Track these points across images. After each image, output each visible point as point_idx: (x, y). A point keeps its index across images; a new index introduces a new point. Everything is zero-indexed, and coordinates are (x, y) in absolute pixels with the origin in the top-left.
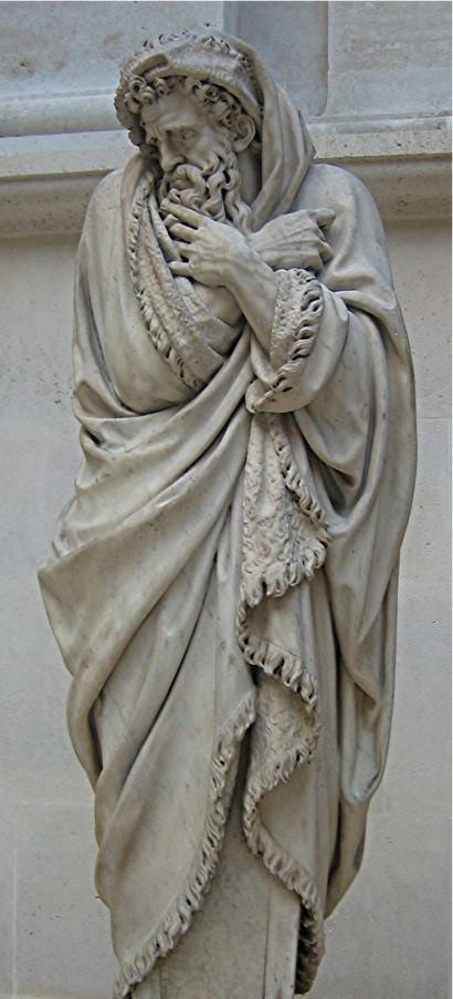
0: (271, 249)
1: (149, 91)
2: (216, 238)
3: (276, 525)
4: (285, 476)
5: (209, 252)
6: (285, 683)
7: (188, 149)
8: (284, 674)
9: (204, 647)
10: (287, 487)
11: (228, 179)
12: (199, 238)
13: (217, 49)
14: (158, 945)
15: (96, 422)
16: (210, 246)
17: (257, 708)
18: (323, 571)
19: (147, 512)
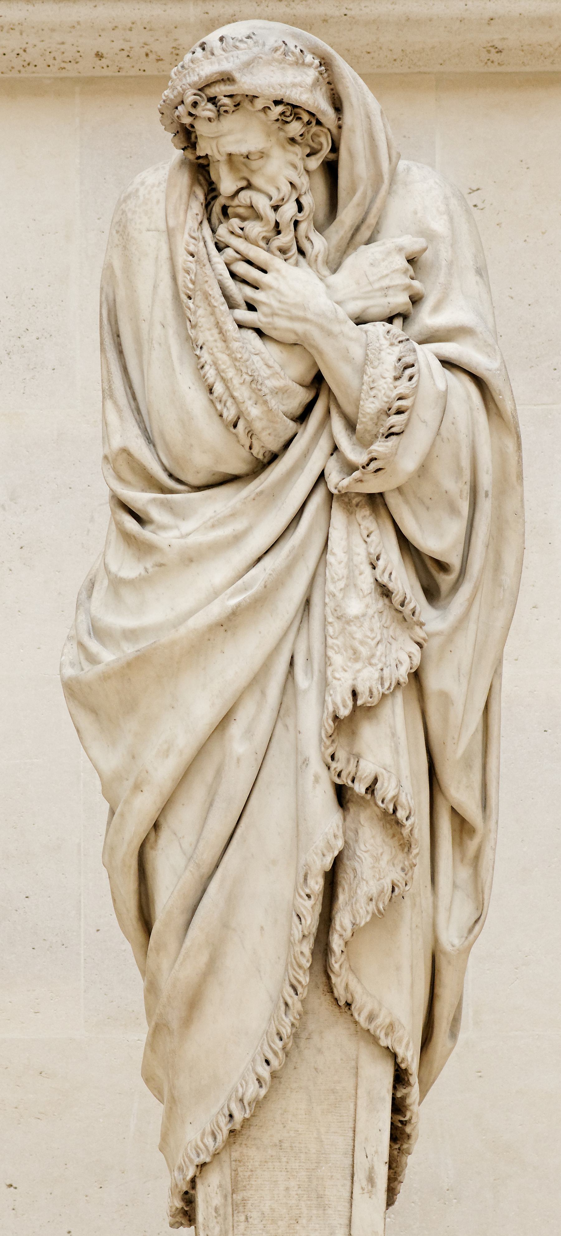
0: (355, 299)
1: (210, 110)
2: (294, 287)
3: (366, 624)
4: (374, 568)
5: (285, 307)
6: (380, 803)
7: (253, 171)
8: (379, 794)
9: (279, 765)
10: (376, 580)
11: (300, 208)
12: (271, 288)
13: (291, 58)
14: (231, 1116)
15: (140, 498)
16: (283, 299)
17: (344, 833)
18: (416, 676)
19: (216, 610)
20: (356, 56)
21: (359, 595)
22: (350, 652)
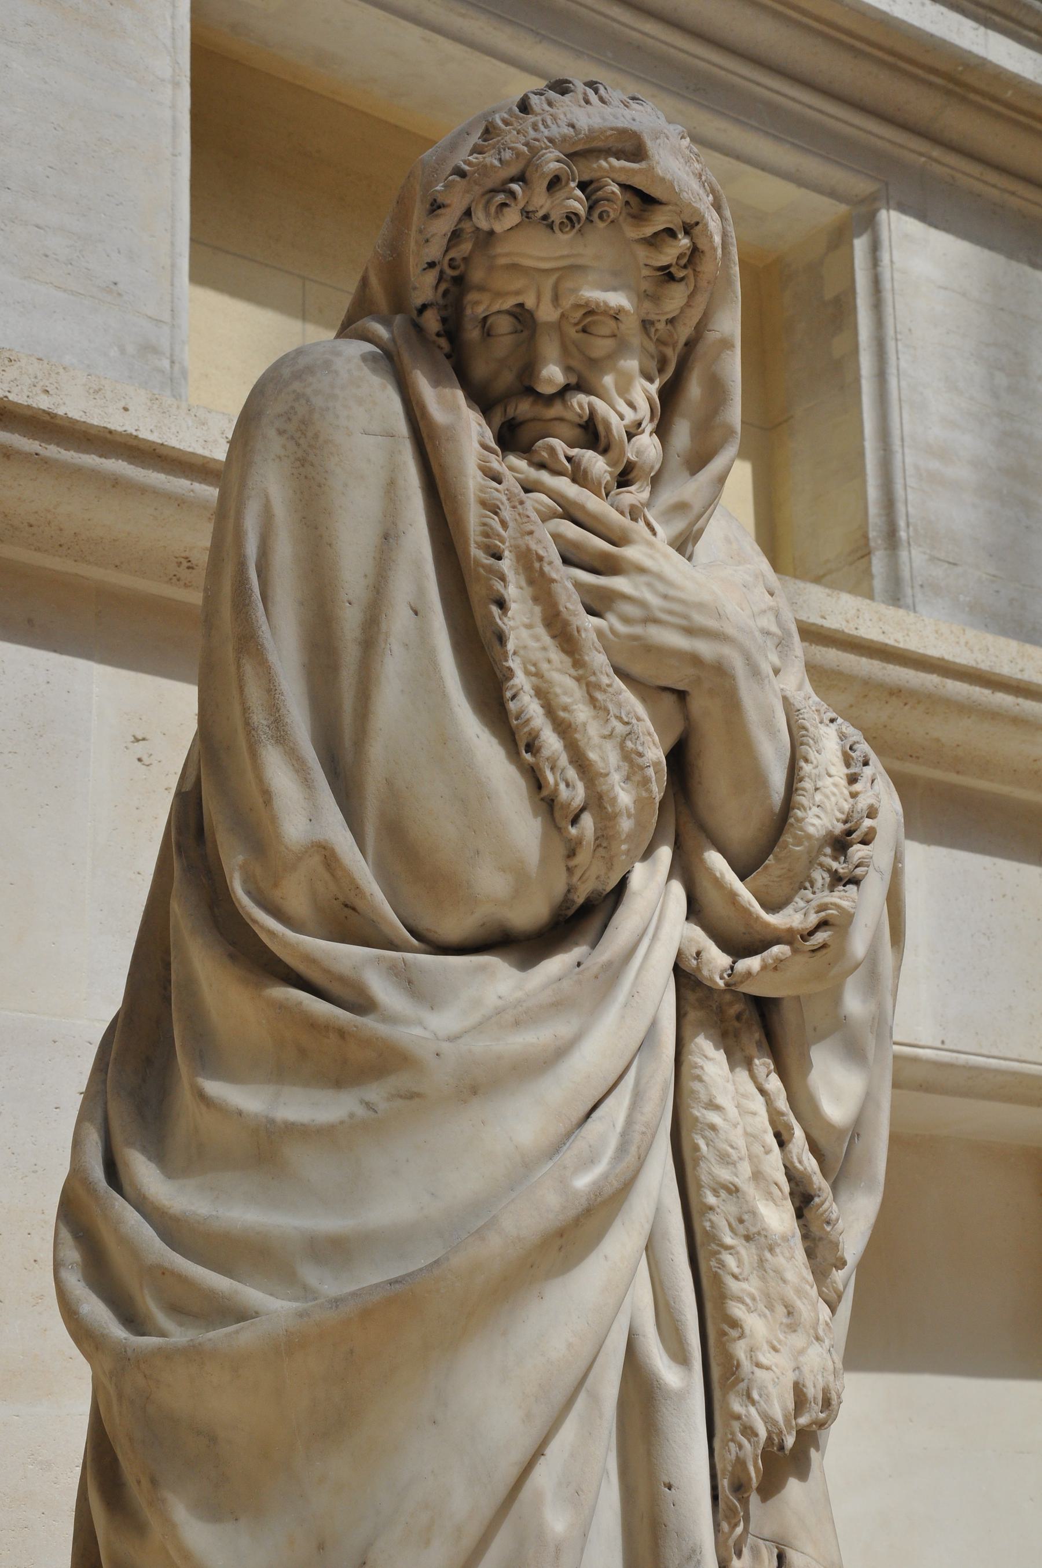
16: (672, 592)
20: (12, 526)
21: (770, 1194)
22: (781, 1310)
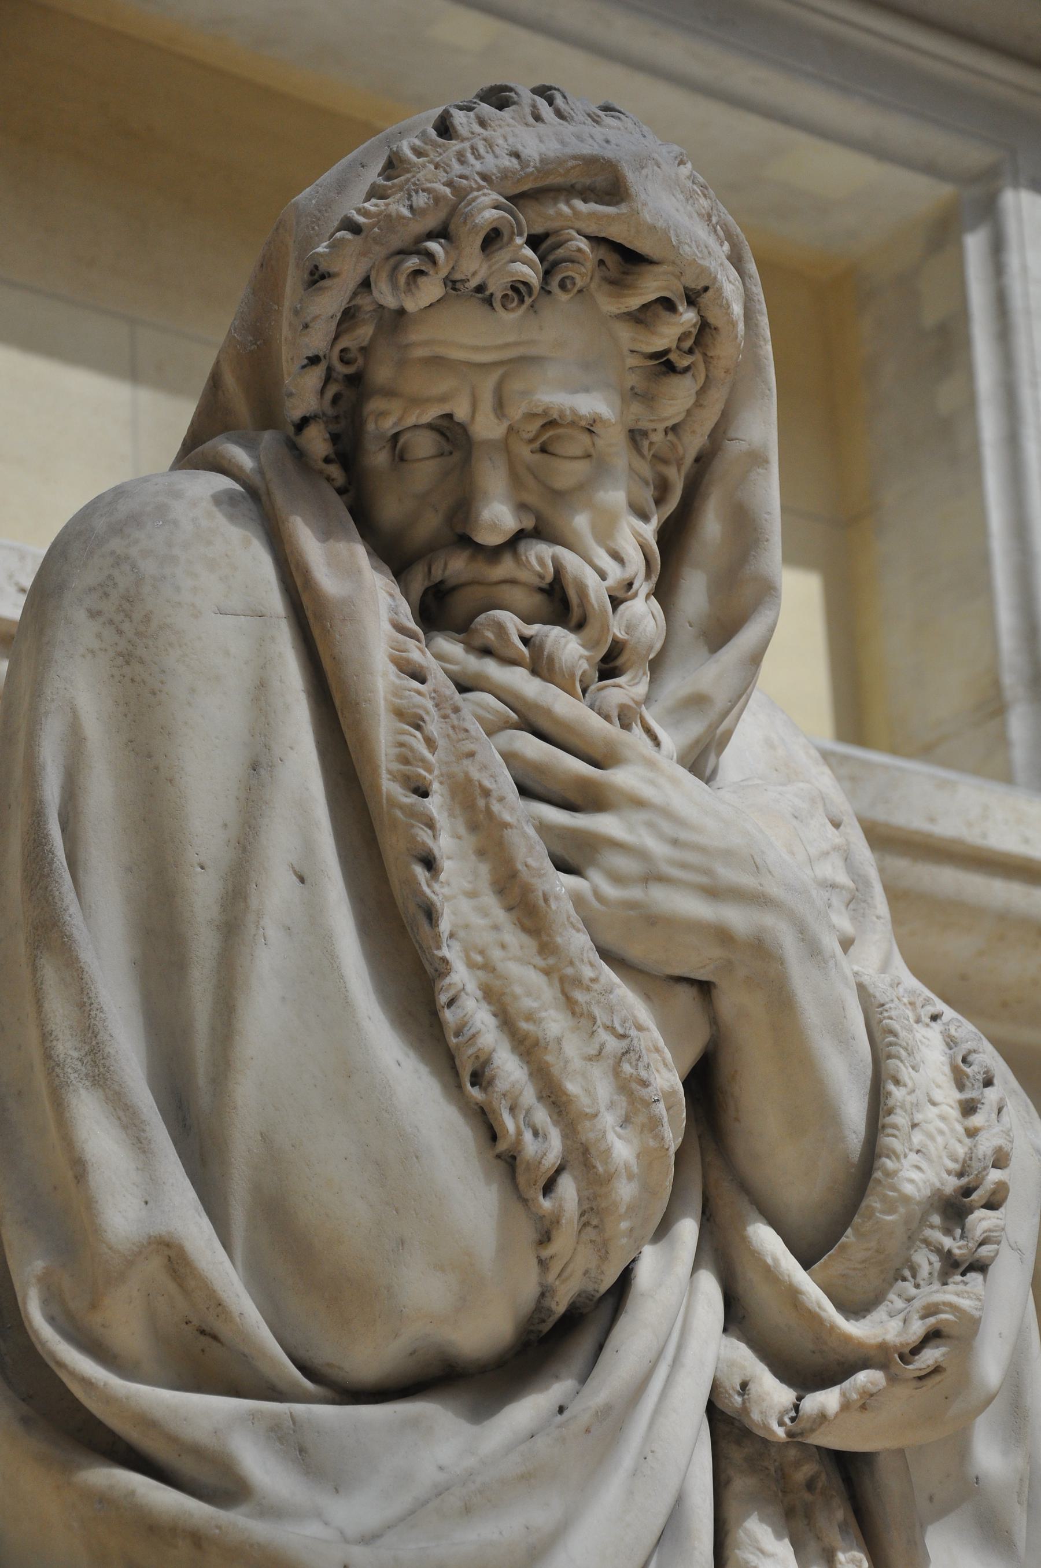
16: (684, 835)
